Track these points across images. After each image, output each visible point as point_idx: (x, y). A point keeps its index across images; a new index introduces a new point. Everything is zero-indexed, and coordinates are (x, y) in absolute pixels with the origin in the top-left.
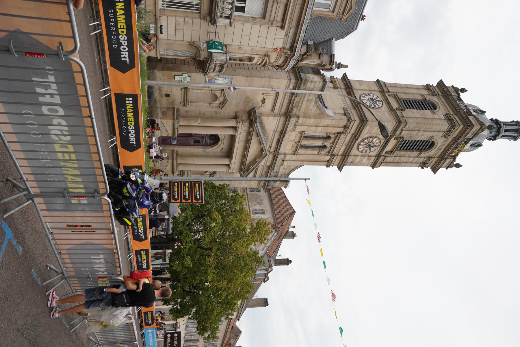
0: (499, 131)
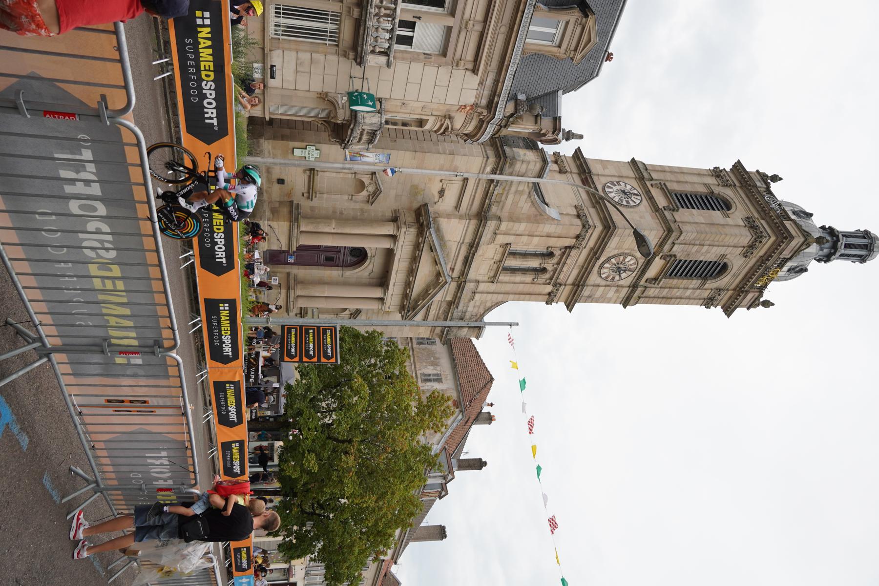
0: (834, 247)
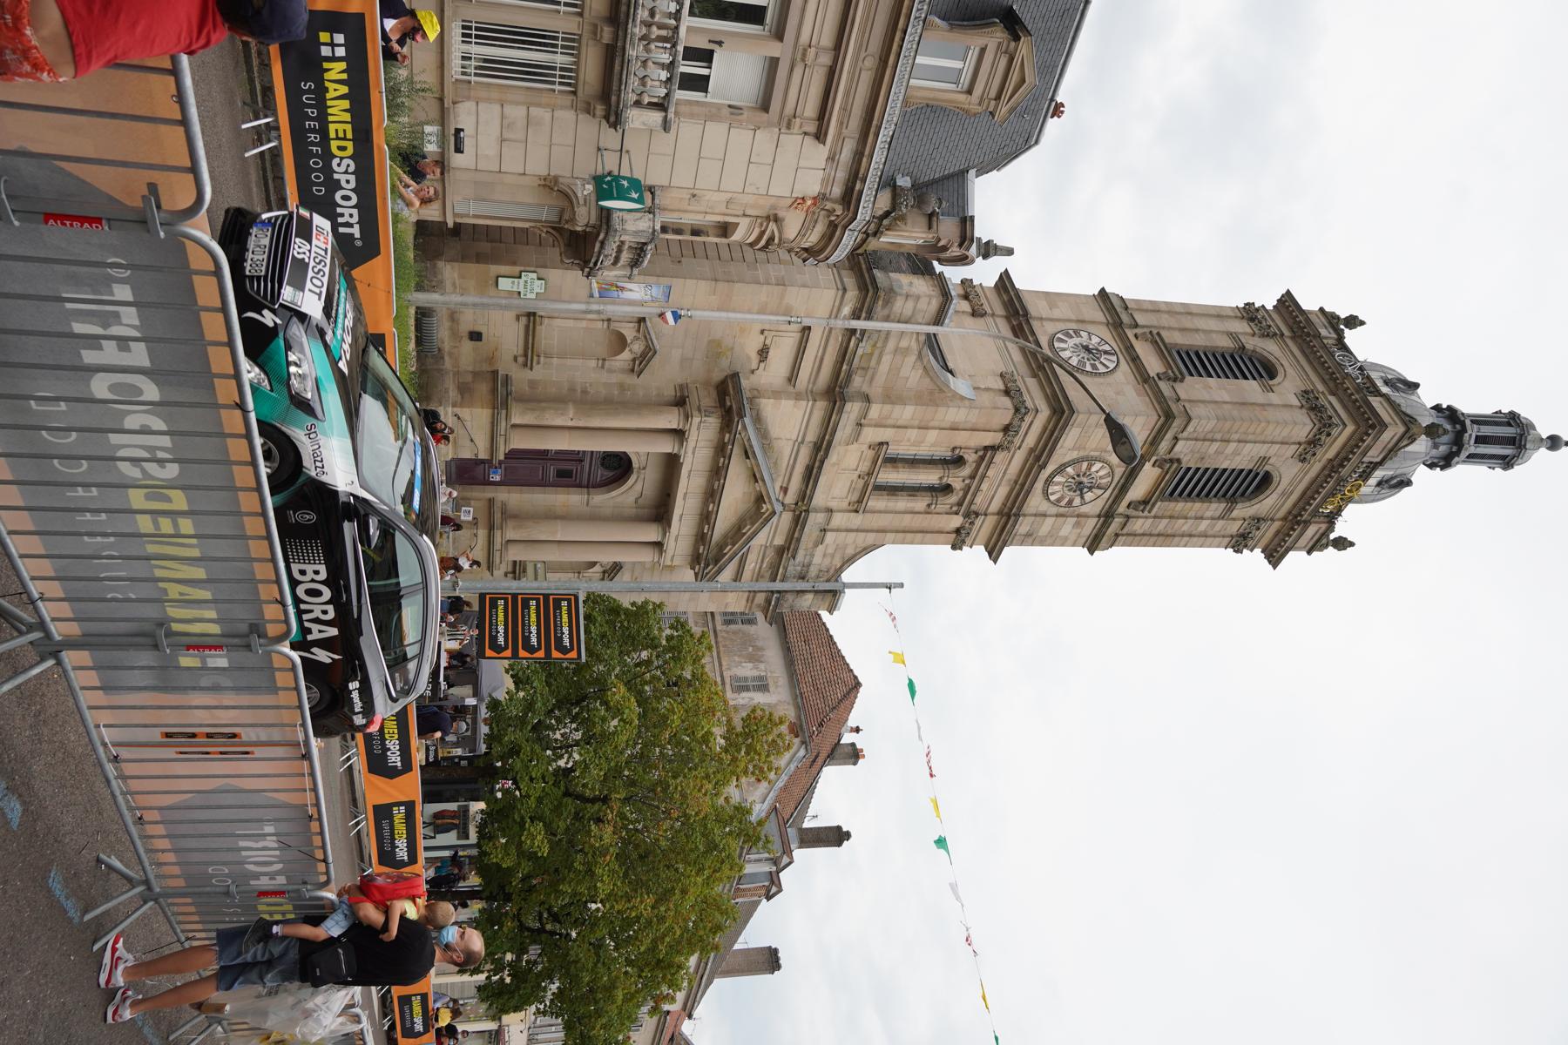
0: (1458, 442)
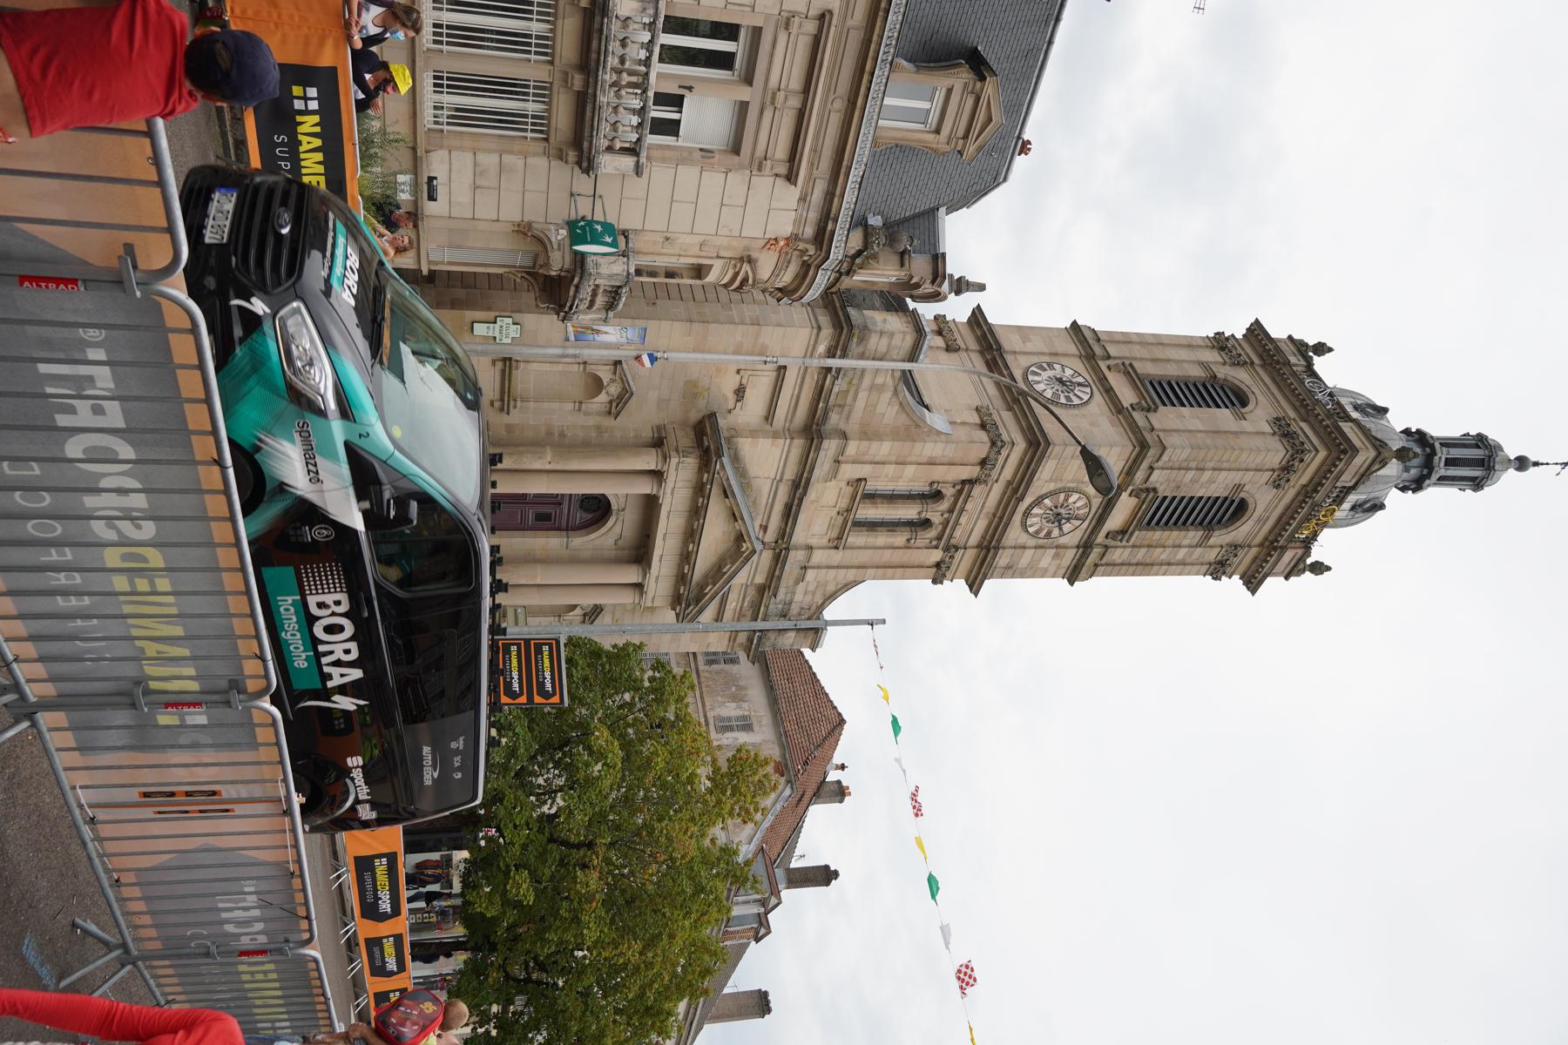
0: (1428, 465)
